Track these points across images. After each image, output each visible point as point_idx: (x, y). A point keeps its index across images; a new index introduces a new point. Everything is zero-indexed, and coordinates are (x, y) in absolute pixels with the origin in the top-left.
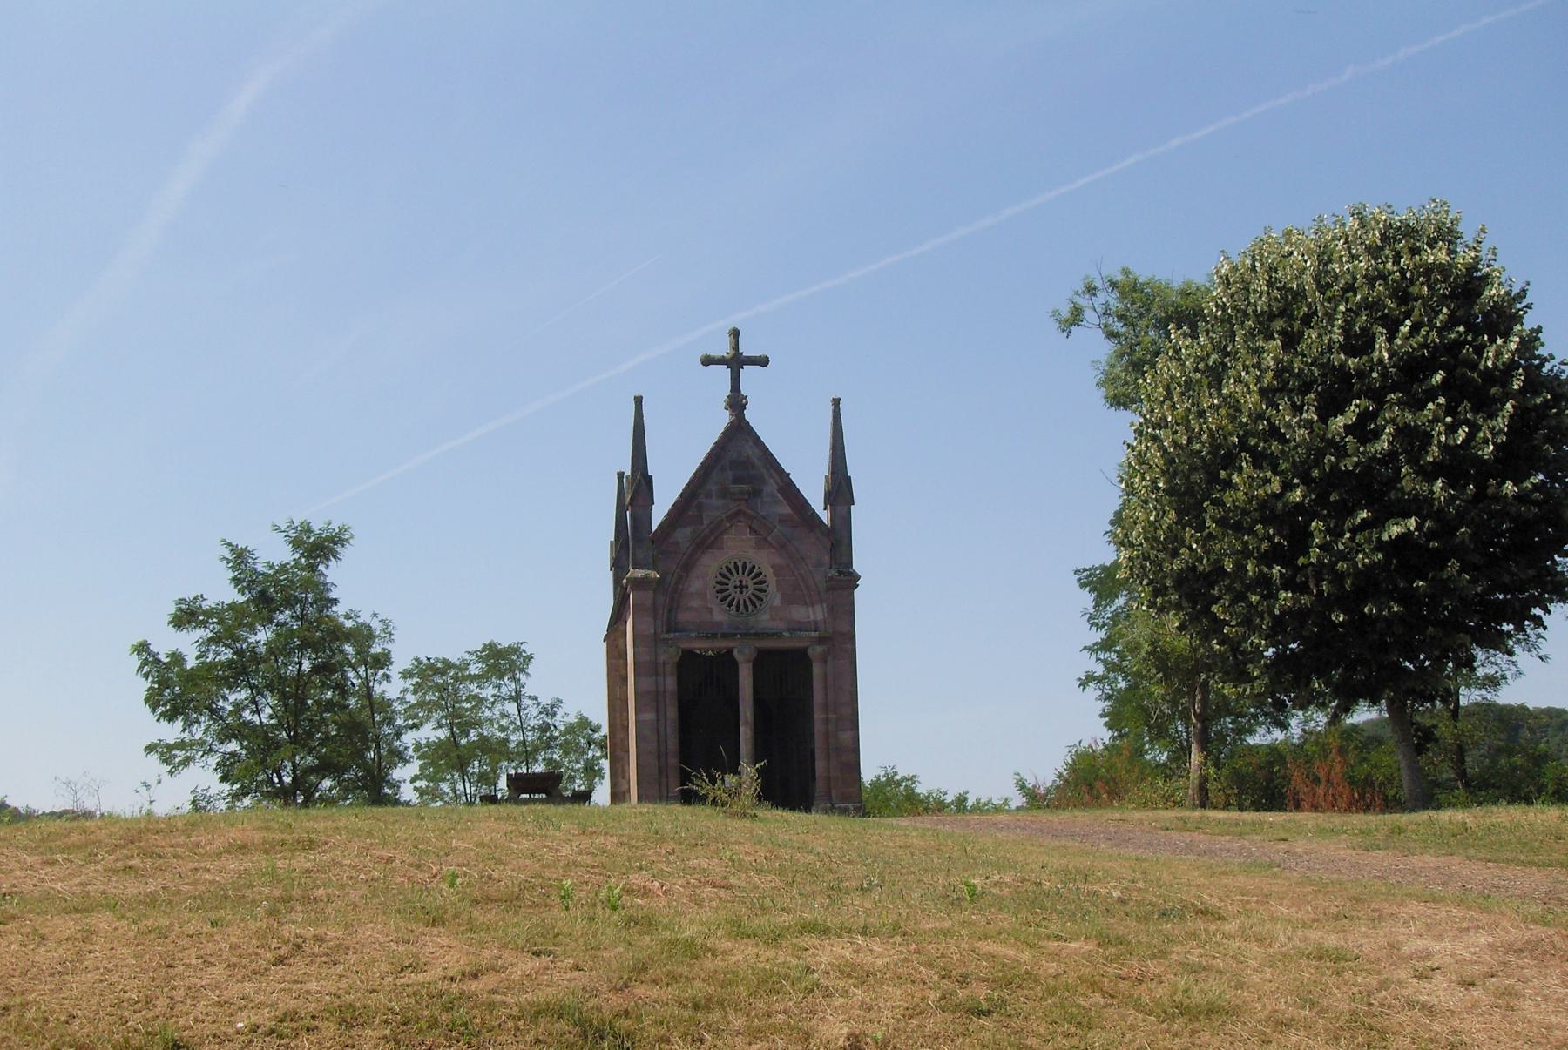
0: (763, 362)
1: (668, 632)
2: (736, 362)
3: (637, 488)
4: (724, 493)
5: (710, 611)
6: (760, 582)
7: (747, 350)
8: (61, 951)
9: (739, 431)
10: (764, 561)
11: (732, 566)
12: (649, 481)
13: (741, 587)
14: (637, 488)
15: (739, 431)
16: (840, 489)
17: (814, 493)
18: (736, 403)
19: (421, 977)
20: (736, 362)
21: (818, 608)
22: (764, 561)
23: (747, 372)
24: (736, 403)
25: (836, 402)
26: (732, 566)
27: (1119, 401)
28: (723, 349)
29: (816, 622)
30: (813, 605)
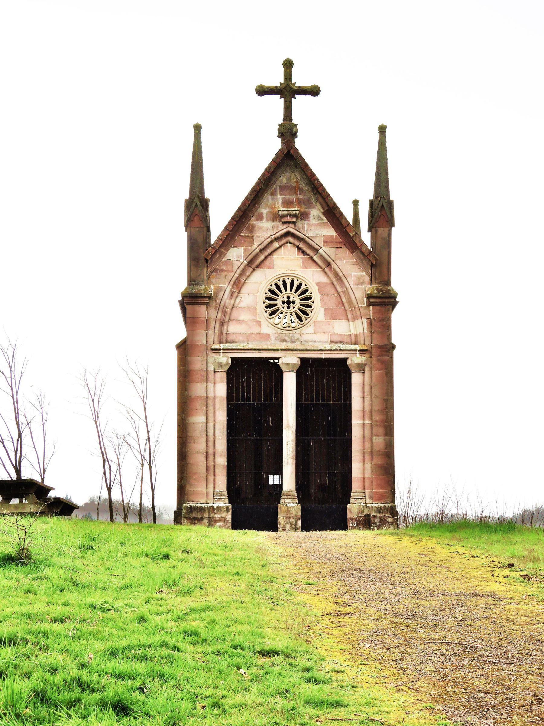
0: (314, 91)
1: (221, 342)
2: (288, 91)
3: (197, 208)
4: (276, 217)
5: (259, 324)
6: (306, 299)
7: (300, 79)
8: (536, 608)
9: (288, 159)
10: (312, 278)
11: (281, 284)
12: (205, 204)
13: (289, 302)
14: (197, 208)
15: (288, 159)
16: (382, 211)
17: (350, 218)
18: (288, 132)
19: (108, 653)
20: (288, 91)
21: (358, 322)
22: (312, 278)
23: (298, 101)
24: (288, 132)
25: (382, 130)
26: (281, 284)
27: (369, 231)
28: (276, 79)
29: (356, 336)
30: (354, 319)
